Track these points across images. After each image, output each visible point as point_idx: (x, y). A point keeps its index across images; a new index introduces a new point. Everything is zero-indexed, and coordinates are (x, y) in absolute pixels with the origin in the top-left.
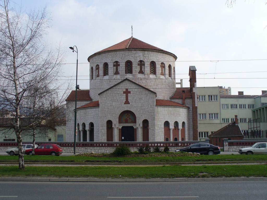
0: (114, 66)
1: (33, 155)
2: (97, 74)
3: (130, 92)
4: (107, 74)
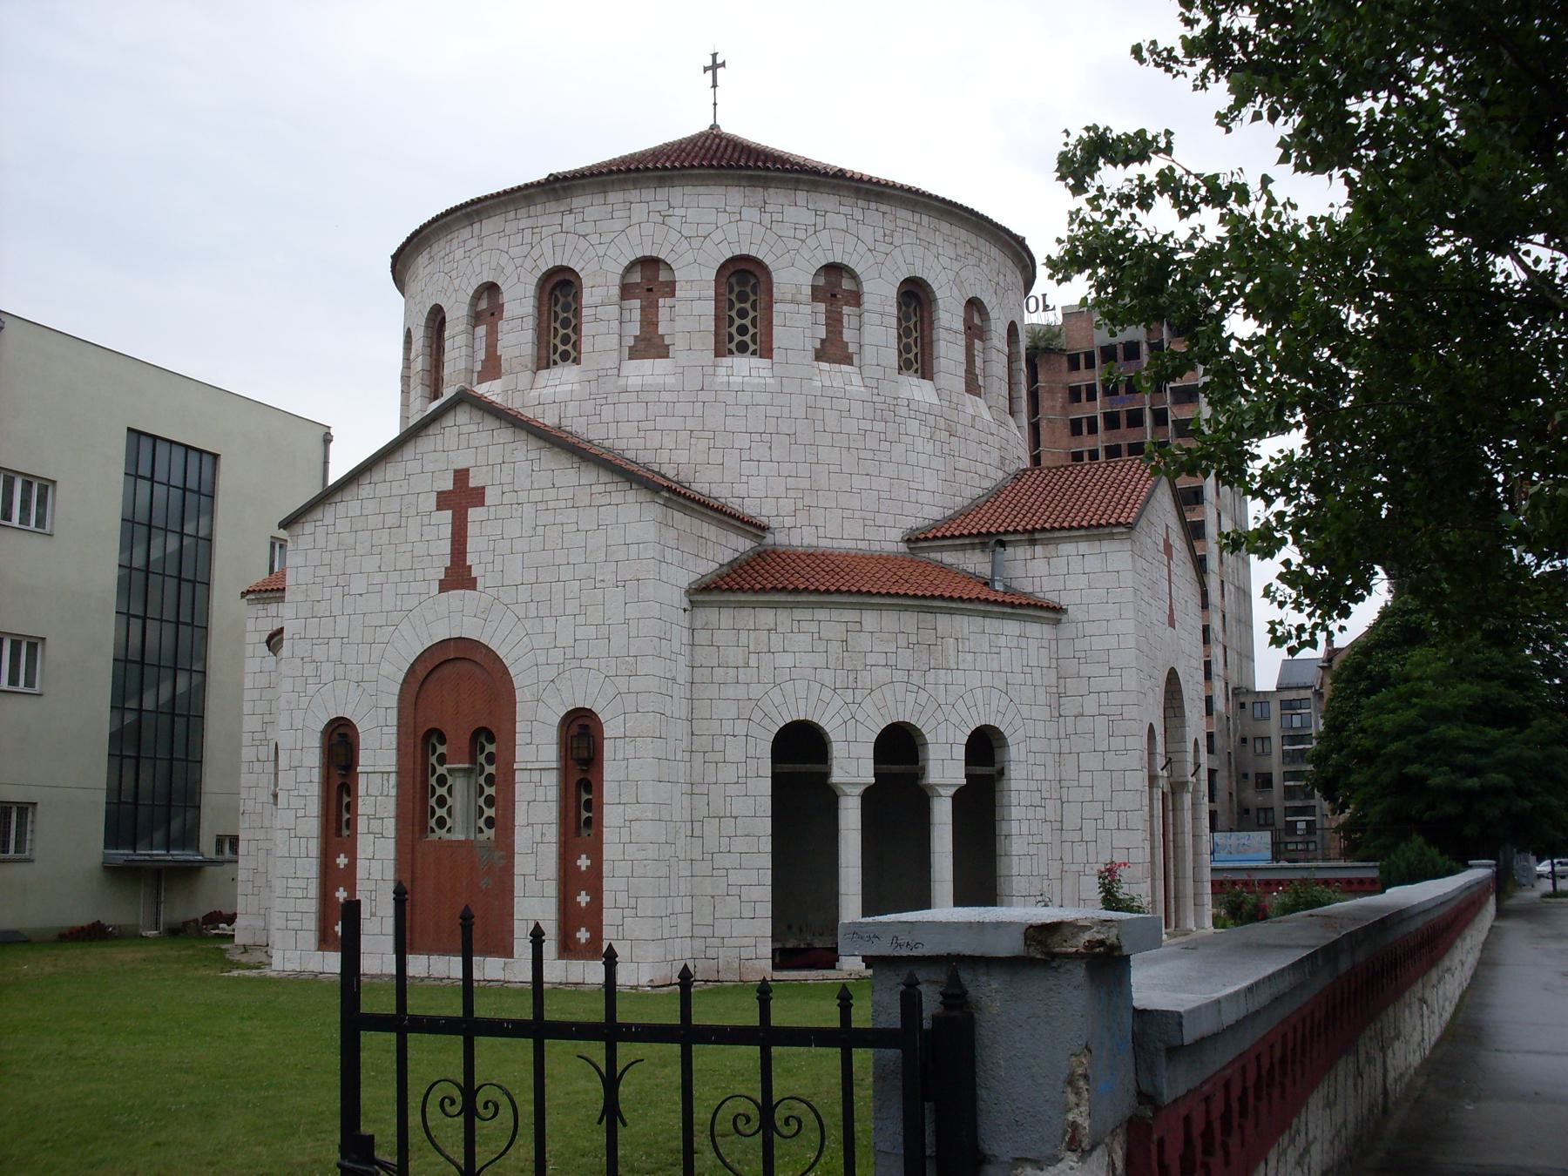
0: (626, 291)
1: (449, 813)
2: (482, 355)
4: (571, 355)
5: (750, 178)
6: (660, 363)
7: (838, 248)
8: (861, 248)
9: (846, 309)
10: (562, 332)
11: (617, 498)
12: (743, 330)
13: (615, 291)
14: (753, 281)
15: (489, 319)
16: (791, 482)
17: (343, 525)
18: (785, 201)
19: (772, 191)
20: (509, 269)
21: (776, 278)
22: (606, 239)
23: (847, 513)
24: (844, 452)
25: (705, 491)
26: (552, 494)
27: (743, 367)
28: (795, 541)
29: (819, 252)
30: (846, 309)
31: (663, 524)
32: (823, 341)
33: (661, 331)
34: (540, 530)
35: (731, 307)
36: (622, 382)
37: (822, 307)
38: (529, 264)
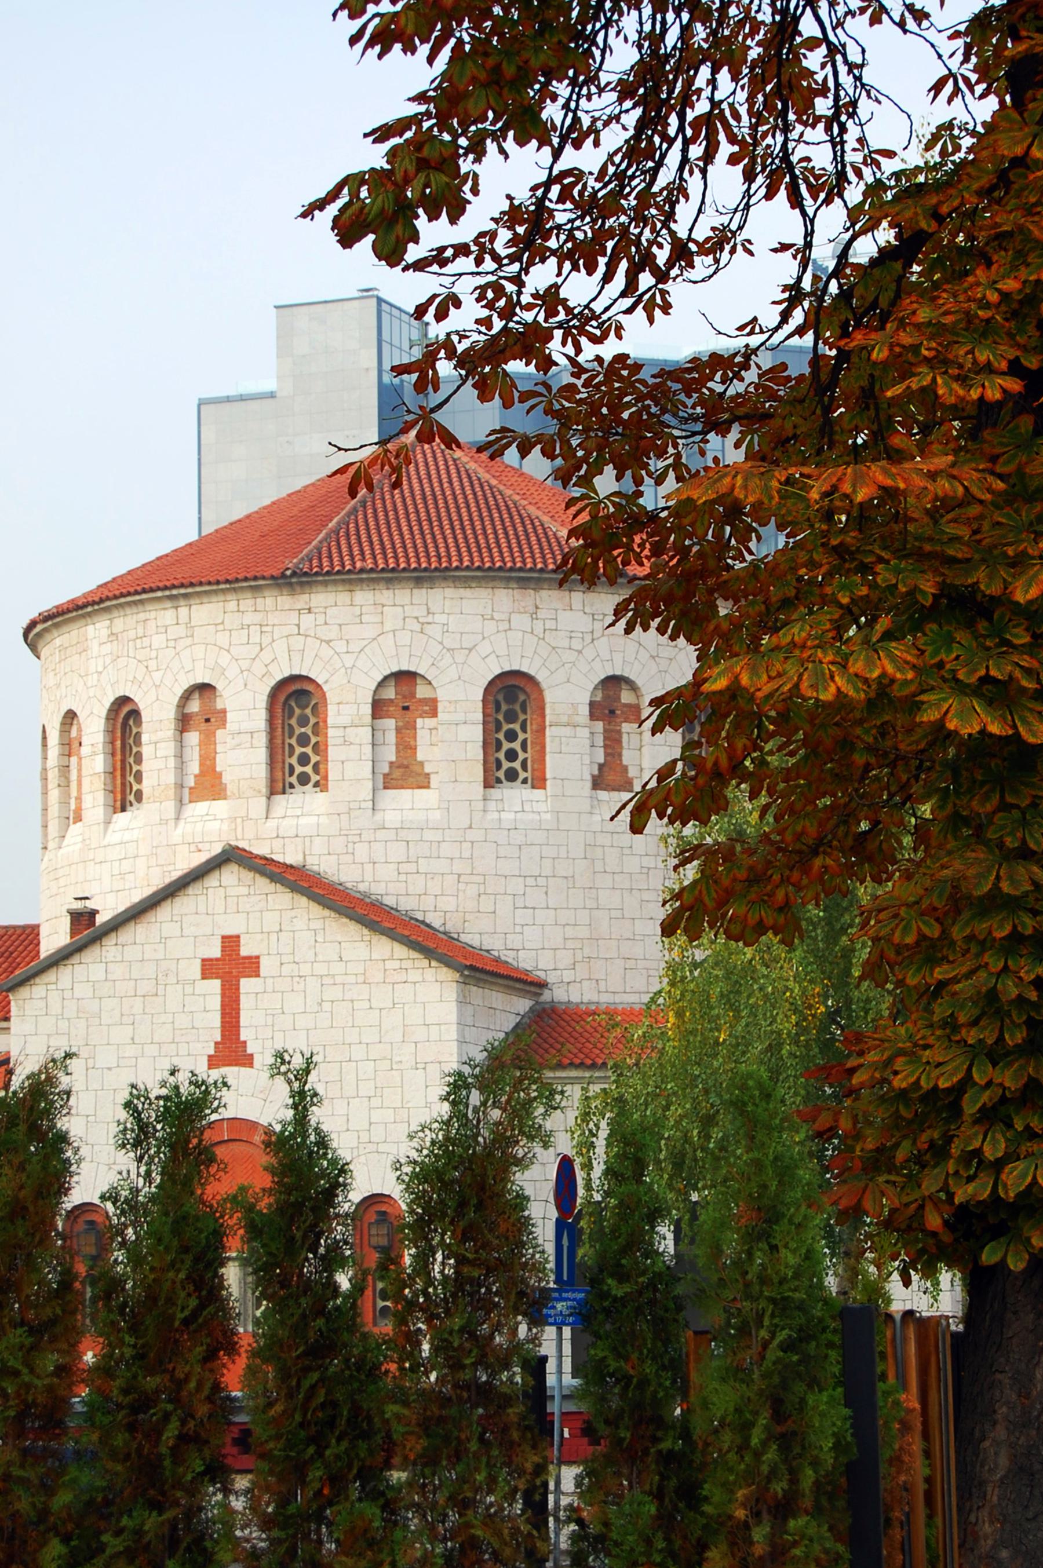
0: (379, 708)
3: (252, 966)
5: (520, 580)
6: (421, 794)
7: (618, 658)
8: (644, 655)
9: (626, 727)
10: (299, 750)
11: (414, 975)
12: (512, 755)
13: (368, 710)
14: (522, 697)
15: (204, 726)
16: (570, 932)
17: (82, 990)
18: (559, 606)
19: (544, 593)
20: (232, 672)
21: (549, 697)
22: (355, 647)
23: (630, 964)
24: (626, 894)
25: (476, 943)
26: (338, 968)
27: (514, 796)
28: (575, 998)
29: (597, 665)
30: (626, 727)
31: (463, 1001)
32: (601, 767)
33: (420, 757)
34: (327, 1006)
35: (498, 729)
36: (379, 816)
37: (599, 726)
38: (258, 668)
